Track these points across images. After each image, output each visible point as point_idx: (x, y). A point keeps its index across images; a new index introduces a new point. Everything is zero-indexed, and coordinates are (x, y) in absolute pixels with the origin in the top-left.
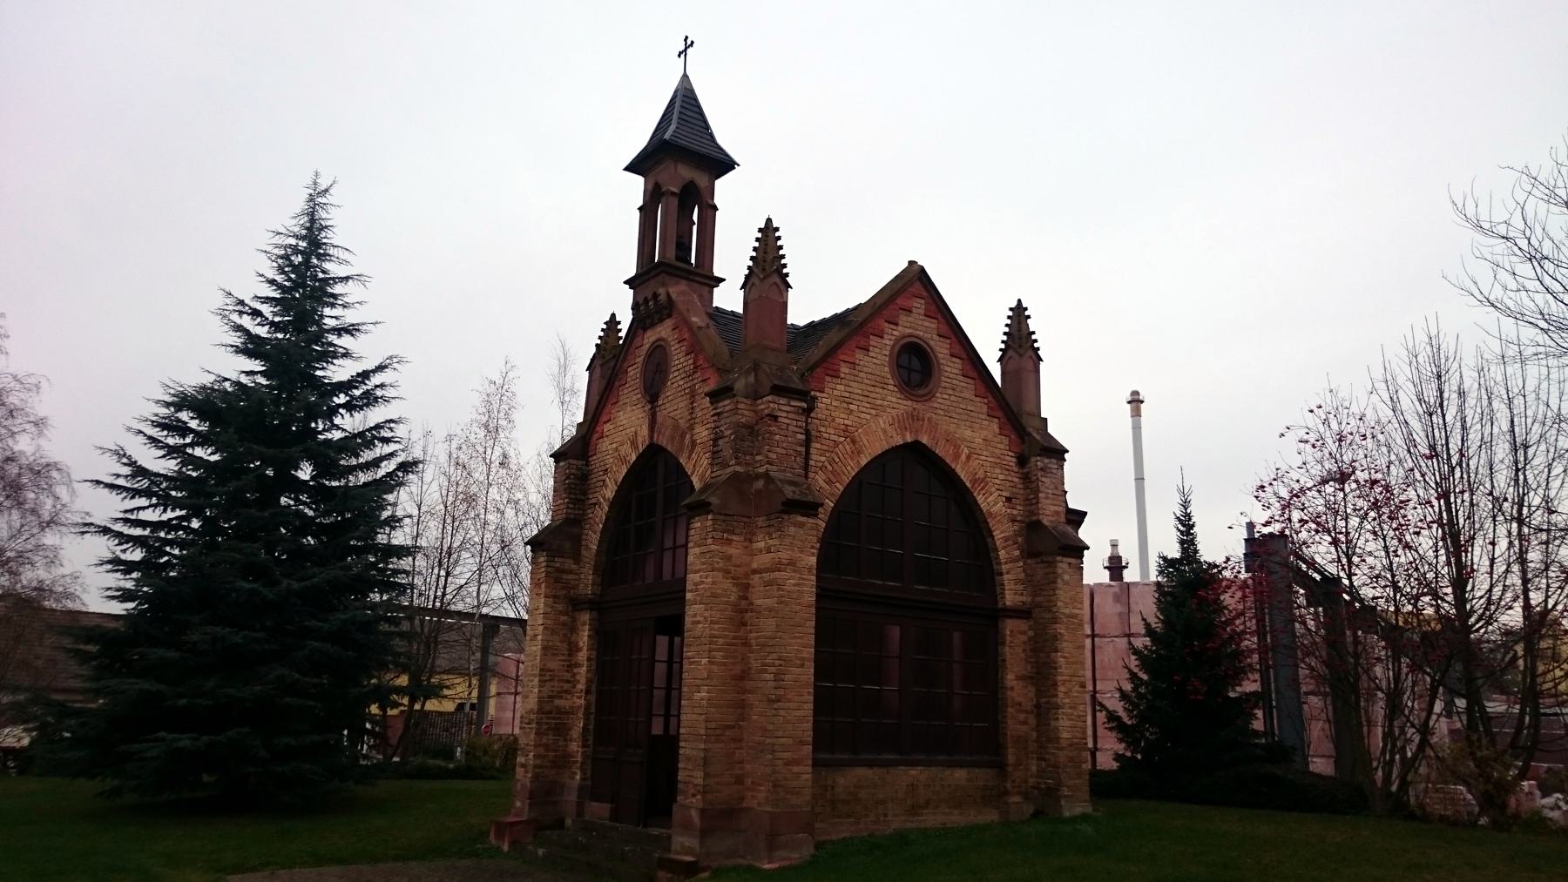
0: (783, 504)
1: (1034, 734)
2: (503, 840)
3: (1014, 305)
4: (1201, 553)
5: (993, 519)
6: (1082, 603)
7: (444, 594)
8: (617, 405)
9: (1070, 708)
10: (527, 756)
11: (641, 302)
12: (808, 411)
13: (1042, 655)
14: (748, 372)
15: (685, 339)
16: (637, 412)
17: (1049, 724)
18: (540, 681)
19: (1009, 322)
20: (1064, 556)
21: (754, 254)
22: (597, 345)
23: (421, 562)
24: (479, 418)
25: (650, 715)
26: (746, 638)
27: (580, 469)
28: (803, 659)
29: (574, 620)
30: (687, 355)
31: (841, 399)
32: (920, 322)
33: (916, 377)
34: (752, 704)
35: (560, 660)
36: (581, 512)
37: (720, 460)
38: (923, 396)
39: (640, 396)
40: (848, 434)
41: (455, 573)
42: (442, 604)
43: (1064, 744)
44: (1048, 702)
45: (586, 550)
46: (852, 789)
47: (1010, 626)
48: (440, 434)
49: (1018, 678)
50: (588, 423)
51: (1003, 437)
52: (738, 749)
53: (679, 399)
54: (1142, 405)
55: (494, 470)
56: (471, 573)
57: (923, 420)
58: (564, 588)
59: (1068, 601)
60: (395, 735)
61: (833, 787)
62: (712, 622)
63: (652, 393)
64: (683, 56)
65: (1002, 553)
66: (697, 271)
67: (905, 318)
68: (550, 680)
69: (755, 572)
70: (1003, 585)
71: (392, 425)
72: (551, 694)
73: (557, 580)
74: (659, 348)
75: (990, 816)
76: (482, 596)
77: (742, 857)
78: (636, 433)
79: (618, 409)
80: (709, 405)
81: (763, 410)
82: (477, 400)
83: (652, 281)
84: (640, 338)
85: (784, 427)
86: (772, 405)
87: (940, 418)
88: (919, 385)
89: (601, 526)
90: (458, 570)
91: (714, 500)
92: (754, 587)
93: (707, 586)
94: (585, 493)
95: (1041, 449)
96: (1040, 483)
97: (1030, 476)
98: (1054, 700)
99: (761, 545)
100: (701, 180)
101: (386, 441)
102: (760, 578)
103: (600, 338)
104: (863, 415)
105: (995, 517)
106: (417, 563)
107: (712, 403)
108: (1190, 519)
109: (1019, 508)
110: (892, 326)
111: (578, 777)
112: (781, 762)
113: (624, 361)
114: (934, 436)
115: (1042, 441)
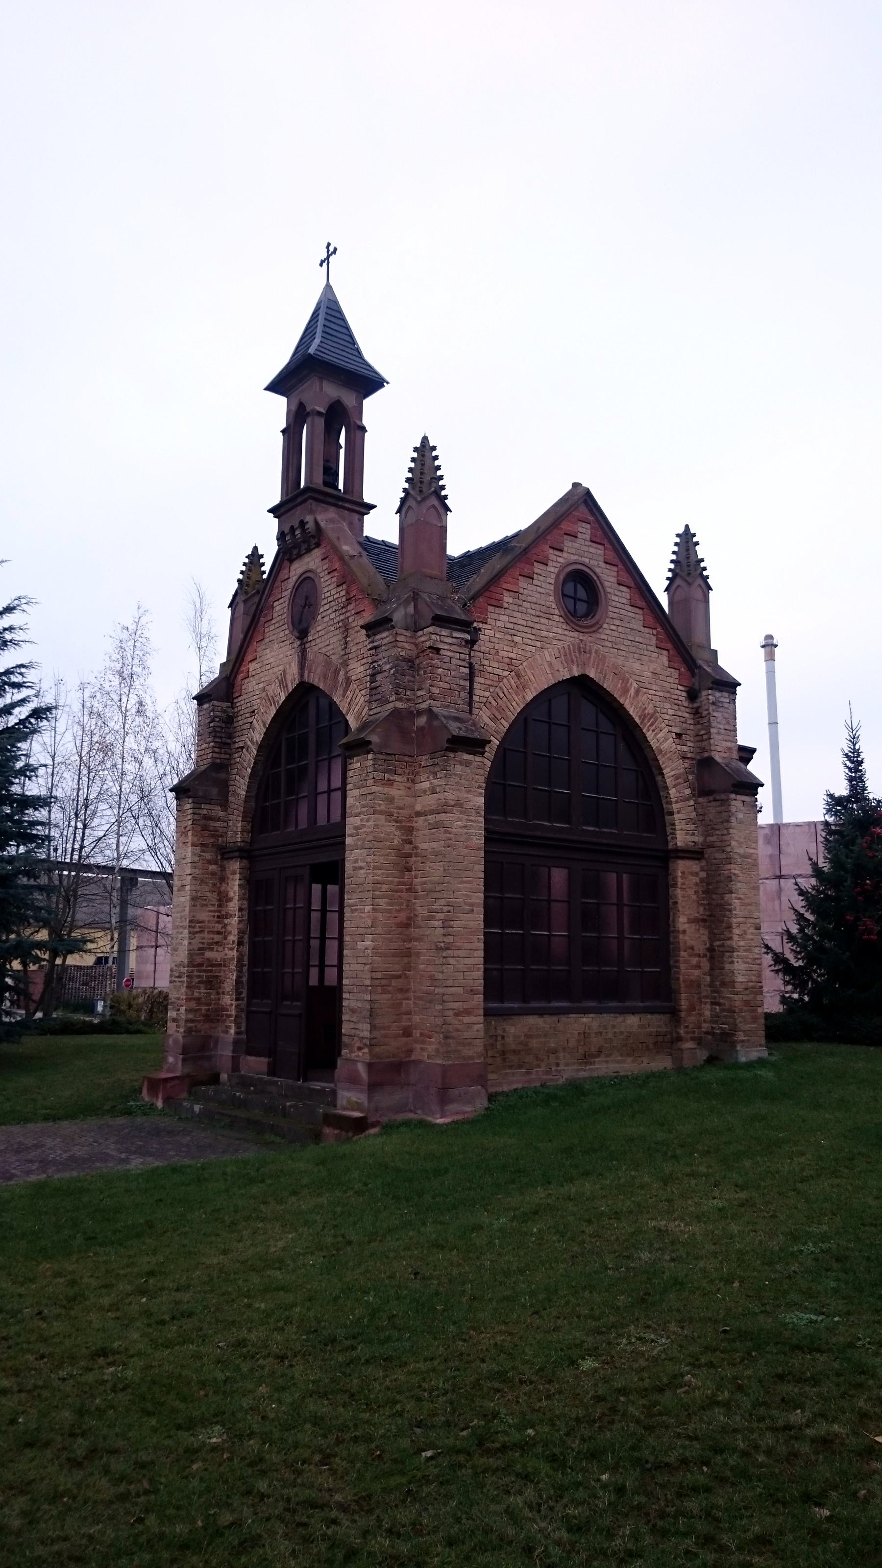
0: (449, 741)
1: (708, 978)
2: (157, 1098)
3: (681, 530)
4: (869, 789)
5: (663, 756)
6: (756, 842)
7: (82, 847)
8: (264, 642)
9: (745, 951)
10: (178, 1010)
11: (287, 530)
12: (472, 643)
13: (714, 896)
14: (406, 603)
15: (336, 570)
16: (284, 649)
17: (723, 968)
18: (190, 933)
19: (676, 549)
20: (737, 793)
21: (410, 475)
22: (239, 581)
23: (57, 815)
24: (112, 665)
25: (308, 966)
26: (411, 884)
27: (225, 711)
28: (472, 905)
29: (223, 869)
30: (338, 586)
31: (505, 630)
32: (586, 549)
33: (582, 608)
34: (418, 953)
35: (210, 911)
36: (227, 756)
37: (378, 696)
38: (591, 626)
39: (287, 632)
40: (513, 668)
41: (92, 825)
42: (80, 857)
43: (739, 987)
44: (722, 946)
45: (233, 795)
46: (523, 1038)
47: (681, 867)
48: (71, 683)
49: (690, 921)
50: (231, 664)
51: (673, 670)
52: (404, 999)
53: (332, 634)
54: (776, 650)
55: (130, 719)
56: (109, 825)
57: (590, 653)
58: (213, 836)
59: (743, 840)
60: (37, 991)
61: (503, 1037)
62: (375, 868)
63: (302, 632)
64: (325, 265)
65: (672, 792)
66: (347, 496)
67: (570, 544)
68: (200, 932)
69: (418, 814)
70: (674, 824)
71: (23, 670)
72: (201, 946)
73: (205, 828)
74: (307, 580)
75: (662, 1063)
76: (121, 848)
77: (411, 1111)
78: (284, 671)
79: (264, 647)
80: (364, 638)
81: (423, 642)
82: (110, 646)
83: (299, 507)
84: (286, 571)
85: (447, 660)
86: (433, 637)
87: (607, 650)
88: (586, 616)
89: (249, 770)
90: (96, 822)
91: (374, 739)
92: (418, 830)
93: (369, 830)
94: (231, 736)
95: (713, 683)
96: (712, 718)
97: (700, 711)
98: (728, 943)
99: (425, 785)
100: (348, 399)
101: (18, 686)
102: (426, 820)
103: (242, 572)
104: (528, 648)
105: (666, 754)
106: (53, 816)
107: (368, 636)
108: (859, 756)
109: (689, 744)
110: (557, 553)
111: (232, 1031)
112: (451, 1013)
113: (270, 595)
114: (602, 670)
115: (713, 674)
